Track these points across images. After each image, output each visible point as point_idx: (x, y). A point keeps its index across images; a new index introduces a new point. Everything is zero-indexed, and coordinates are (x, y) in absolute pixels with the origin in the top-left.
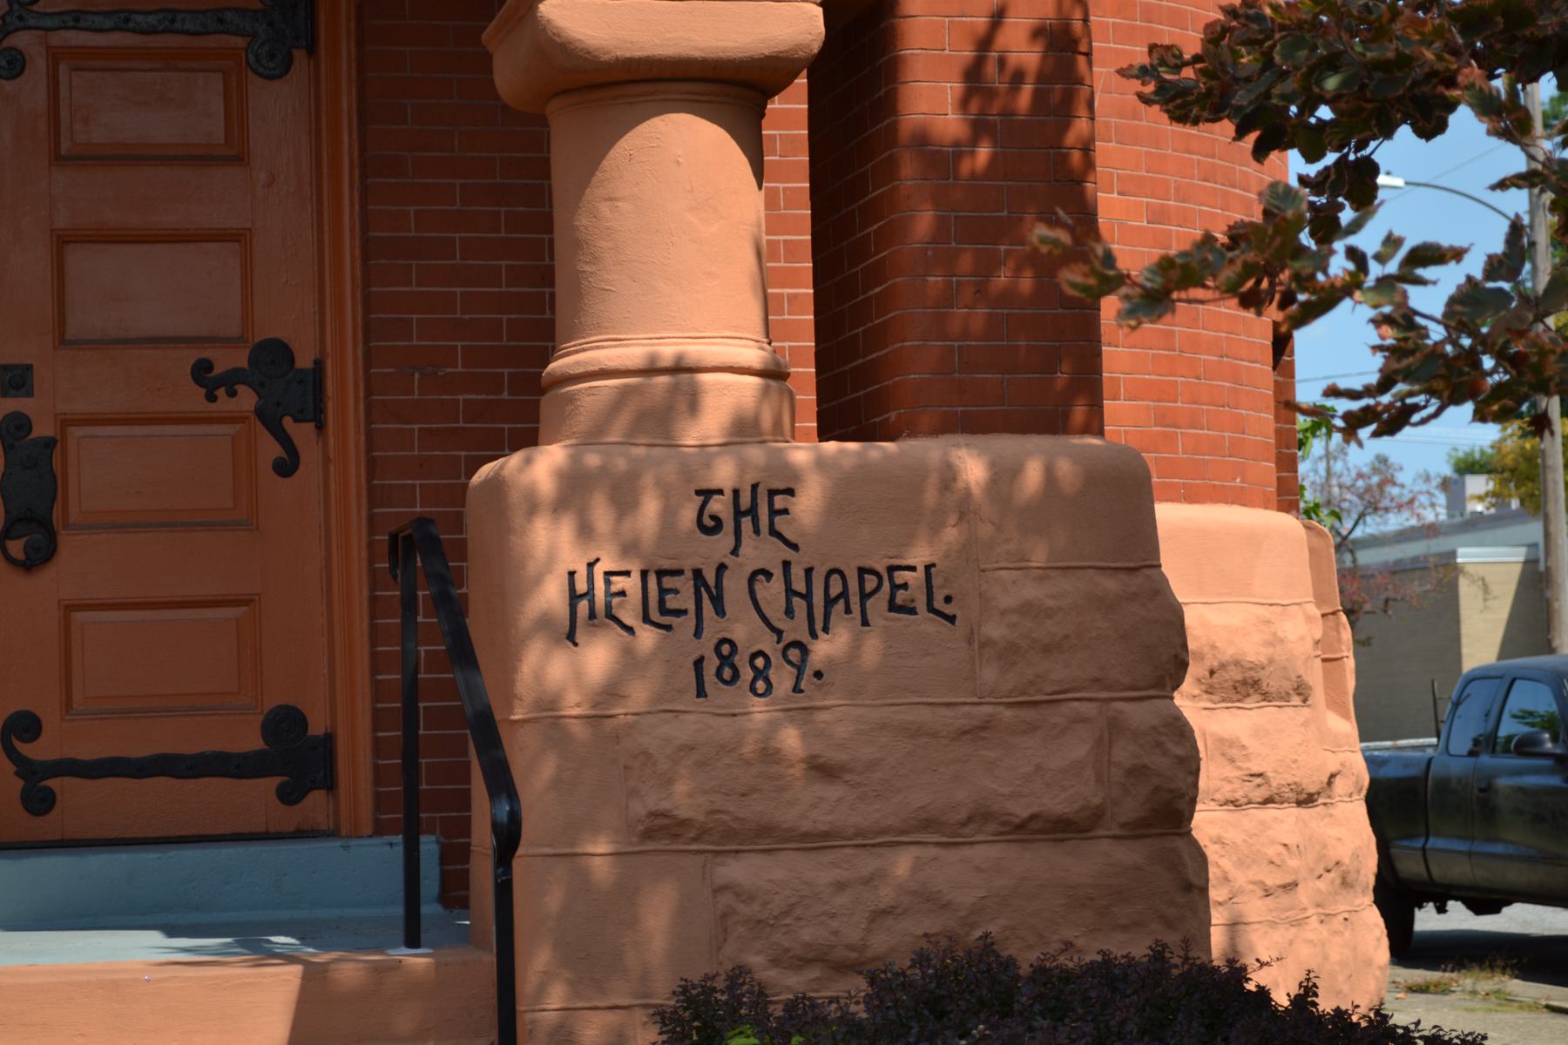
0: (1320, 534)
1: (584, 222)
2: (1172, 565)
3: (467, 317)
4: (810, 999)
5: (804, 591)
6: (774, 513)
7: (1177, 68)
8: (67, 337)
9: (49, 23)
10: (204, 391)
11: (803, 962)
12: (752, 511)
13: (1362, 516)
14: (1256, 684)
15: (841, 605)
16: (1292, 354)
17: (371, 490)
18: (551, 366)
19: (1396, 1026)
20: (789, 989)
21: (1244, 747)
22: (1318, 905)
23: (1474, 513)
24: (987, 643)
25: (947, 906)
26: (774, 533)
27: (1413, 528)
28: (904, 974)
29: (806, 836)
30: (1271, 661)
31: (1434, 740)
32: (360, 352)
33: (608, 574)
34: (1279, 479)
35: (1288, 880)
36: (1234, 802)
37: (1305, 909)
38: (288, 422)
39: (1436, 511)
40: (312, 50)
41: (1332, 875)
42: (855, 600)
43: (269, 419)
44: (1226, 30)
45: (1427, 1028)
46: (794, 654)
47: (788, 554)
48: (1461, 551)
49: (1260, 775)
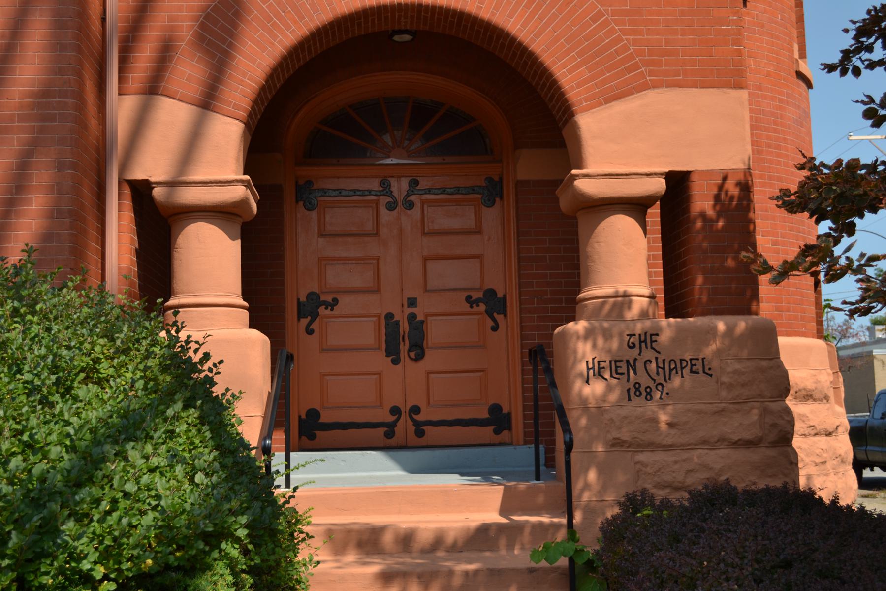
0: (831, 346)
1: (589, 250)
2: (784, 357)
3: (551, 280)
4: (668, 499)
5: (662, 367)
6: (652, 342)
7: (790, 196)
8: (428, 289)
9: (421, 192)
10: (469, 305)
11: (663, 487)
12: (645, 341)
13: (840, 339)
14: (811, 396)
15: (674, 371)
16: (820, 287)
17: (521, 335)
18: (580, 296)
19: (867, 511)
20: (660, 496)
21: (807, 417)
22: (833, 469)
23: (878, 338)
24: (722, 383)
25: (711, 469)
26: (652, 348)
27: (858, 343)
28: (700, 491)
29: (664, 446)
30: (816, 388)
31: (868, 414)
32: (518, 292)
33: (599, 362)
34: (817, 328)
35: (823, 461)
36: (804, 435)
37: (829, 470)
38: (495, 315)
39: (865, 337)
40: (501, 198)
41: (838, 459)
42: (679, 369)
43: (490, 313)
44: (806, 183)
45: (878, 512)
46: (660, 387)
47: (657, 355)
48: (874, 350)
49: (813, 426)
